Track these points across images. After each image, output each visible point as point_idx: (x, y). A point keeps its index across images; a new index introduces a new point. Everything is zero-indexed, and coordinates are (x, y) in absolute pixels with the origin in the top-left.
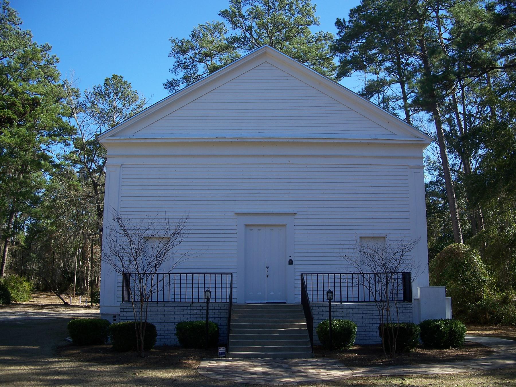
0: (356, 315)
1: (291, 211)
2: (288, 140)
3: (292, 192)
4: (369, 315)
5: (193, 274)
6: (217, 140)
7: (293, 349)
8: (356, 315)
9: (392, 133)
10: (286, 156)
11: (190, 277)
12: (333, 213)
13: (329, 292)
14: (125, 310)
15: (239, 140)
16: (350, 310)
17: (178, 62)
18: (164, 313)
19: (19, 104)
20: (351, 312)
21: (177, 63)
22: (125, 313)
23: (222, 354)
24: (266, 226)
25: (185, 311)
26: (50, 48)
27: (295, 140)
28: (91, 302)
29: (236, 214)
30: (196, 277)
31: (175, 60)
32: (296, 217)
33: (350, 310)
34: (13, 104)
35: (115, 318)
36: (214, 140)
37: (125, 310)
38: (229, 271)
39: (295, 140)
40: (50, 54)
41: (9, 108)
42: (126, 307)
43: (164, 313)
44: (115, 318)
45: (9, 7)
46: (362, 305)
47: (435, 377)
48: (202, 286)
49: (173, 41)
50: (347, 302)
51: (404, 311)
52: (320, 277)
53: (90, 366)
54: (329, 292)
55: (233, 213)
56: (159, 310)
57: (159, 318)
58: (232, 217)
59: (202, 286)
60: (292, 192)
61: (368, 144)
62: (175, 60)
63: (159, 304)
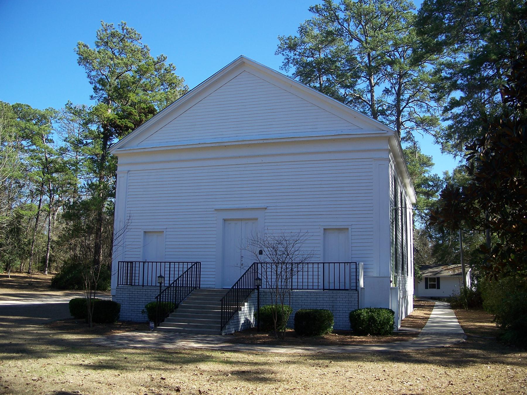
0: (304, 301)
1: (263, 205)
2: (258, 142)
4: (317, 301)
5: (170, 263)
7: (211, 327)
8: (304, 301)
9: (358, 128)
11: (167, 265)
12: (300, 207)
13: (161, 277)
15: (217, 145)
16: (299, 296)
17: (287, 59)
19: (135, 114)
20: (300, 299)
21: (287, 60)
23: (152, 328)
24: (241, 220)
26: (165, 58)
27: (265, 141)
29: (216, 210)
30: (172, 265)
31: (284, 57)
32: (267, 211)
33: (299, 296)
34: (130, 114)
36: (197, 146)
37: (119, 292)
38: (354, 260)
39: (265, 141)
40: (166, 64)
41: (127, 118)
45: (127, 27)
46: (311, 293)
48: (176, 273)
49: (280, 39)
50: (297, 289)
51: (350, 299)
52: (316, 266)
53: (58, 333)
54: (161, 277)
55: (213, 210)
56: (144, 293)
57: (144, 299)
59: (176, 273)
61: (334, 140)
62: (284, 57)
63: (144, 288)
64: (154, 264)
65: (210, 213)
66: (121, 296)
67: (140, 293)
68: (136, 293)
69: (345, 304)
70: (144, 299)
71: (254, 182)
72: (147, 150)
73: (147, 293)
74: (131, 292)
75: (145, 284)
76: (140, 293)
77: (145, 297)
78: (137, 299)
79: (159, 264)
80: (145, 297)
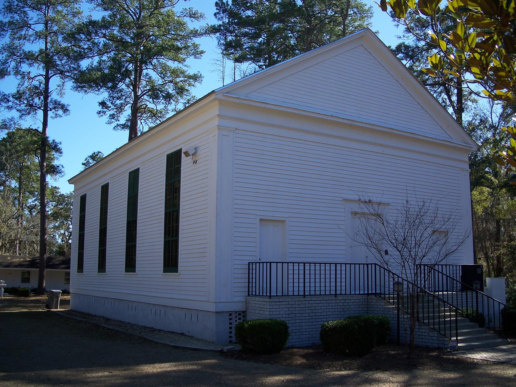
3: (386, 182)
6: (332, 119)
9: (448, 136)
10: (381, 145)
11: (333, 267)
14: (274, 307)
18: (311, 308)
22: (274, 310)
25: (330, 305)
28: (472, 290)
29: (345, 200)
35: (231, 317)
37: (274, 307)
39: (392, 131)
42: (274, 304)
43: (311, 308)
44: (231, 317)
47: (48, 380)
56: (307, 305)
57: (307, 315)
58: (338, 202)
60: (386, 182)
63: (307, 298)
64: (285, 265)
65: (338, 202)
66: (278, 313)
67: (302, 306)
68: (297, 306)
69: (340, 304)
70: (307, 315)
71: (403, 177)
72: (266, 106)
73: (310, 305)
74: (290, 306)
75: (338, 292)
76: (302, 306)
77: (309, 311)
78: (298, 315)
79: (285, 265)
80: (309, 311)
